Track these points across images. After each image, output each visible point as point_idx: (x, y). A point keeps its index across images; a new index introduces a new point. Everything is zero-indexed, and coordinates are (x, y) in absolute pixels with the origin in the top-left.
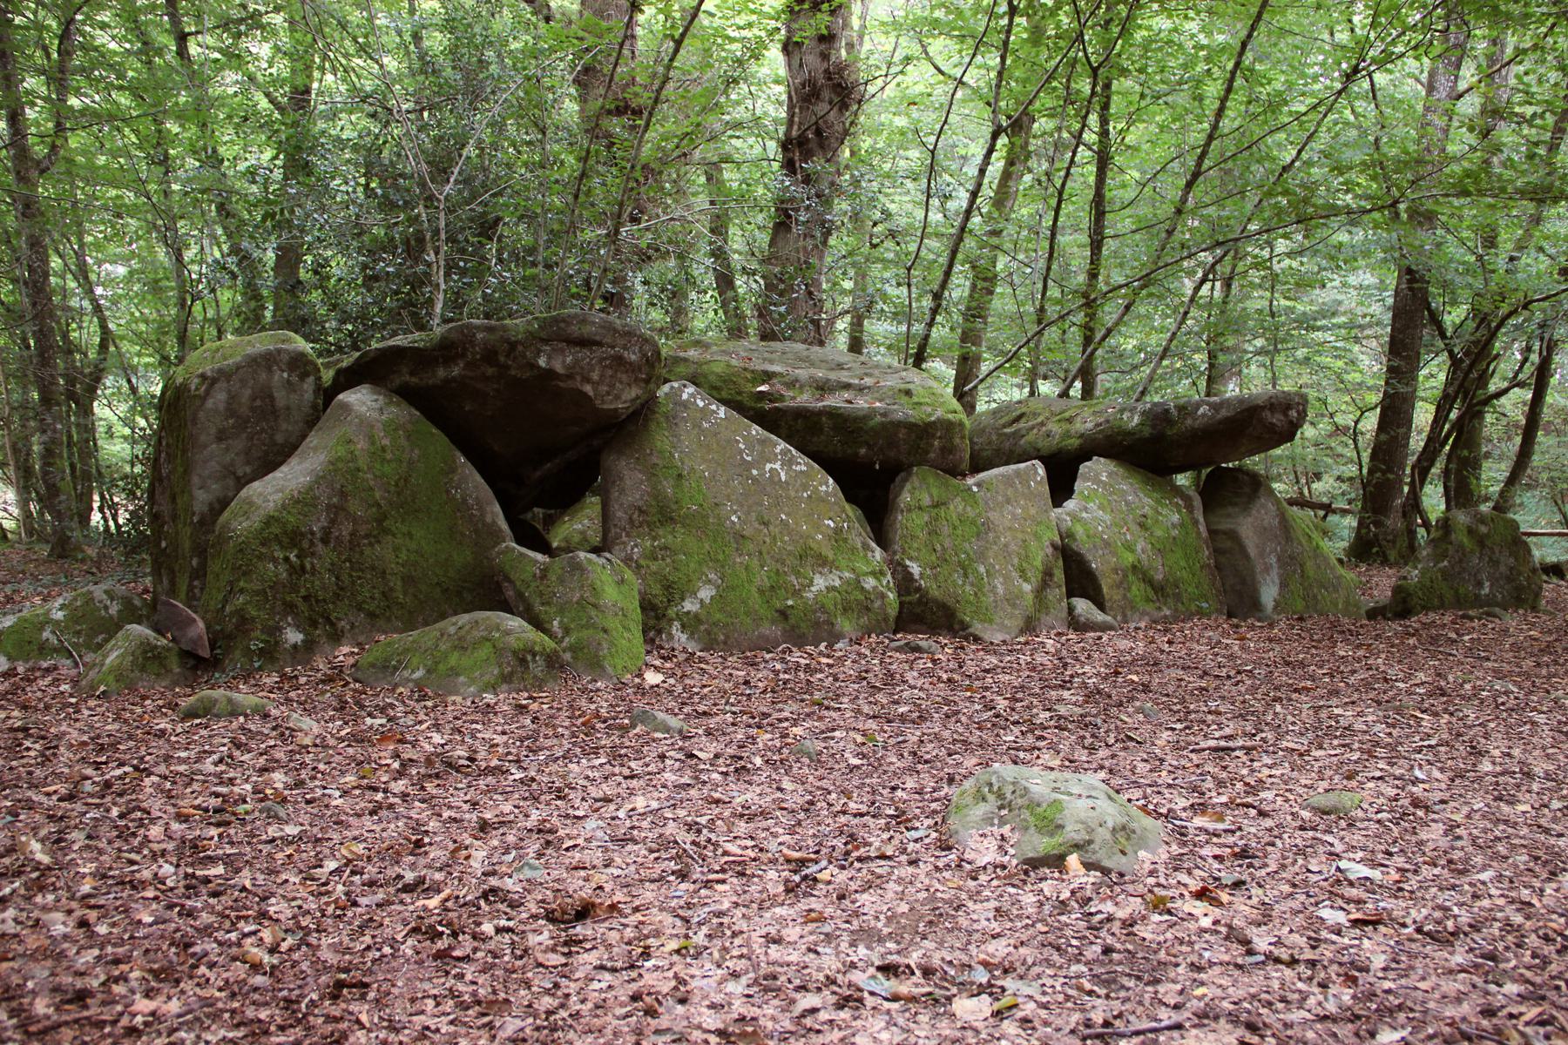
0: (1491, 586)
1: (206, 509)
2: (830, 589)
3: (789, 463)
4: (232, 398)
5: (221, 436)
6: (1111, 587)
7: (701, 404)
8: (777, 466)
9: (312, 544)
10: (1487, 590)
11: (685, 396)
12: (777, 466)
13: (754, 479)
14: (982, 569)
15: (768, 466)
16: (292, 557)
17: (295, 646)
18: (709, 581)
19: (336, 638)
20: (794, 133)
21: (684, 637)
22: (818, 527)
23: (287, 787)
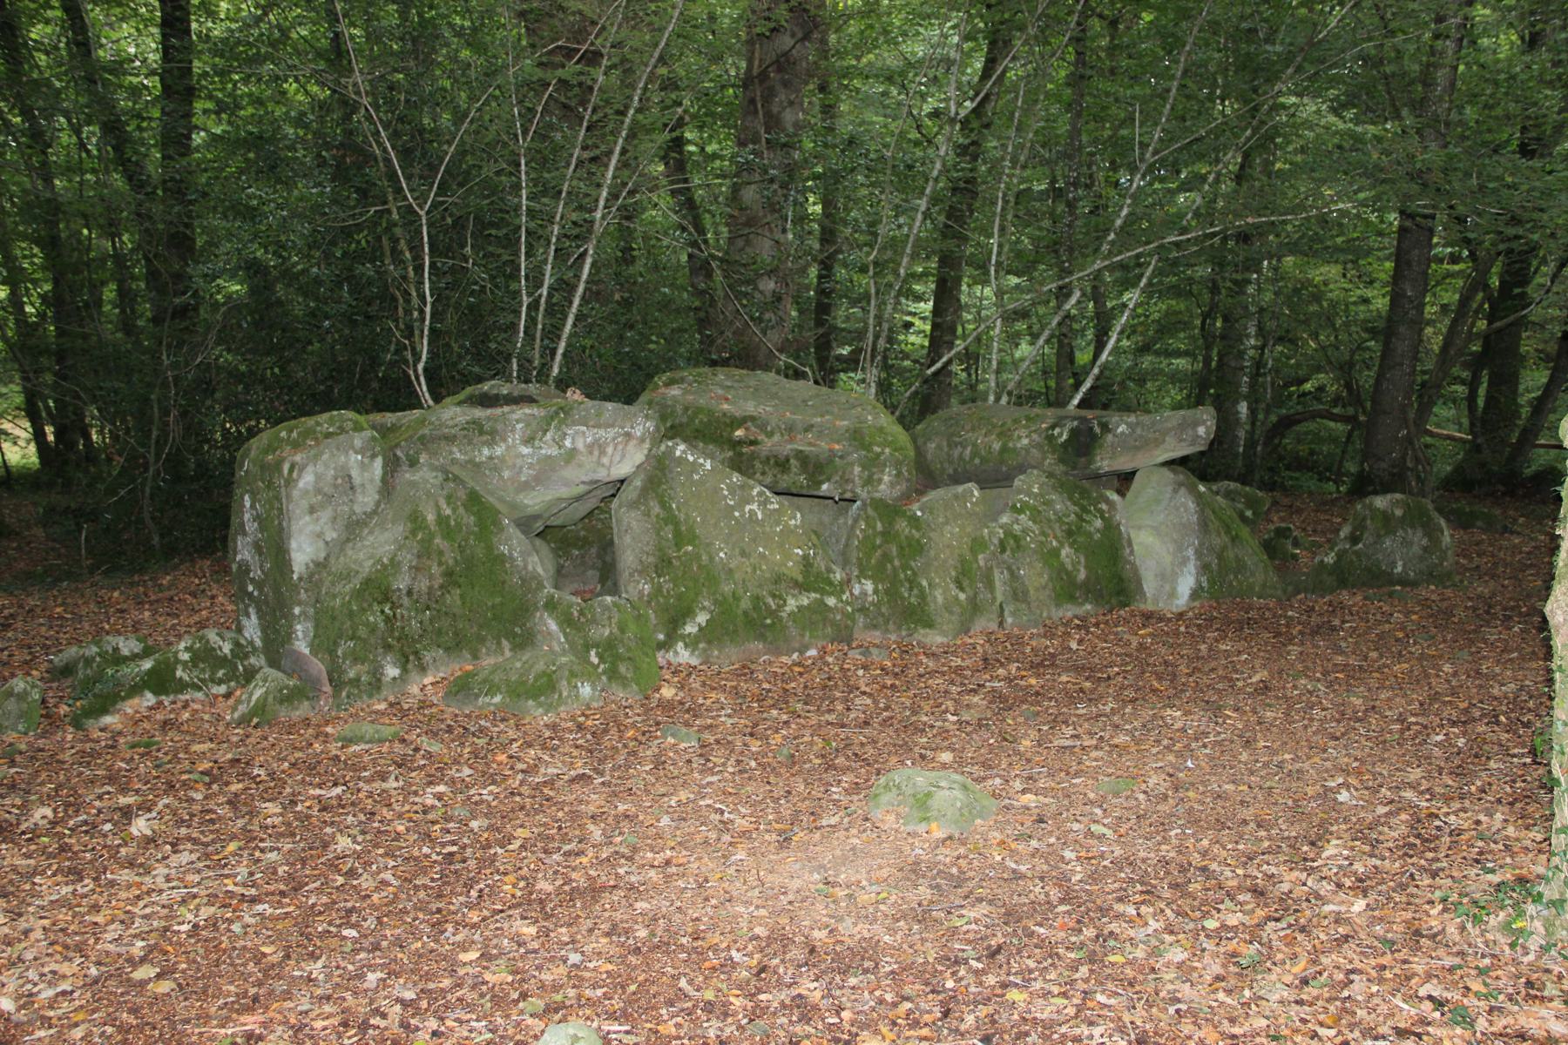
0: (1404, 566)
1: (303, 569)
2: (800, 608)
3: (764, 504)
4: (318, 477)
5: (312, 510)
6: (1037, 590)
7: (691, 458)
8: (755, 507)
9: (400, 597)
10: (1399, 569)
11: (678, 453)
12: (755, 507)
13: (736, 519)
14: (925, 583)
15: (747, 508)
16: (387, 610)
17: (394, 679)
18: (704, 608)
19: (423, 669)
20: (755, 72)
21: (687, 654)
22: (787, 556)
23: (872, 603)
